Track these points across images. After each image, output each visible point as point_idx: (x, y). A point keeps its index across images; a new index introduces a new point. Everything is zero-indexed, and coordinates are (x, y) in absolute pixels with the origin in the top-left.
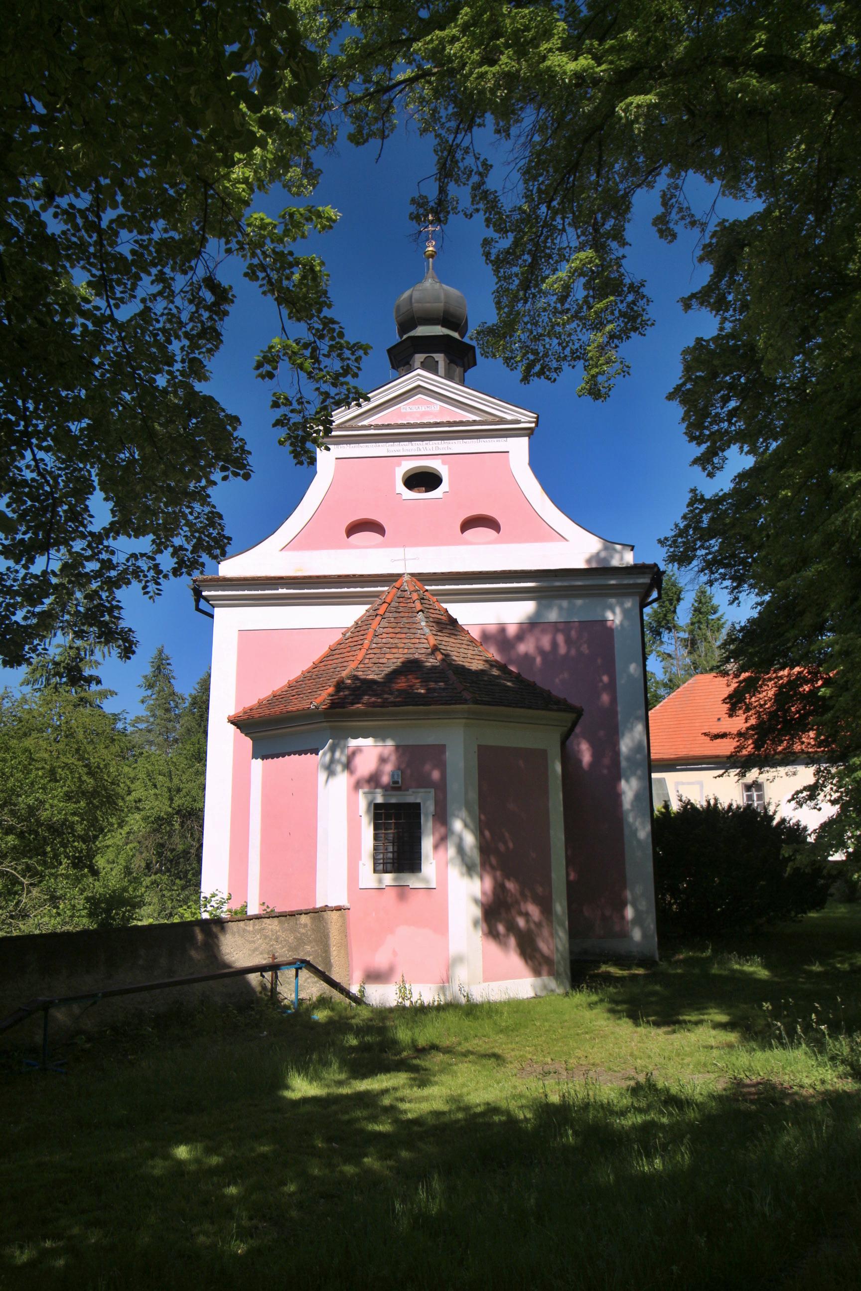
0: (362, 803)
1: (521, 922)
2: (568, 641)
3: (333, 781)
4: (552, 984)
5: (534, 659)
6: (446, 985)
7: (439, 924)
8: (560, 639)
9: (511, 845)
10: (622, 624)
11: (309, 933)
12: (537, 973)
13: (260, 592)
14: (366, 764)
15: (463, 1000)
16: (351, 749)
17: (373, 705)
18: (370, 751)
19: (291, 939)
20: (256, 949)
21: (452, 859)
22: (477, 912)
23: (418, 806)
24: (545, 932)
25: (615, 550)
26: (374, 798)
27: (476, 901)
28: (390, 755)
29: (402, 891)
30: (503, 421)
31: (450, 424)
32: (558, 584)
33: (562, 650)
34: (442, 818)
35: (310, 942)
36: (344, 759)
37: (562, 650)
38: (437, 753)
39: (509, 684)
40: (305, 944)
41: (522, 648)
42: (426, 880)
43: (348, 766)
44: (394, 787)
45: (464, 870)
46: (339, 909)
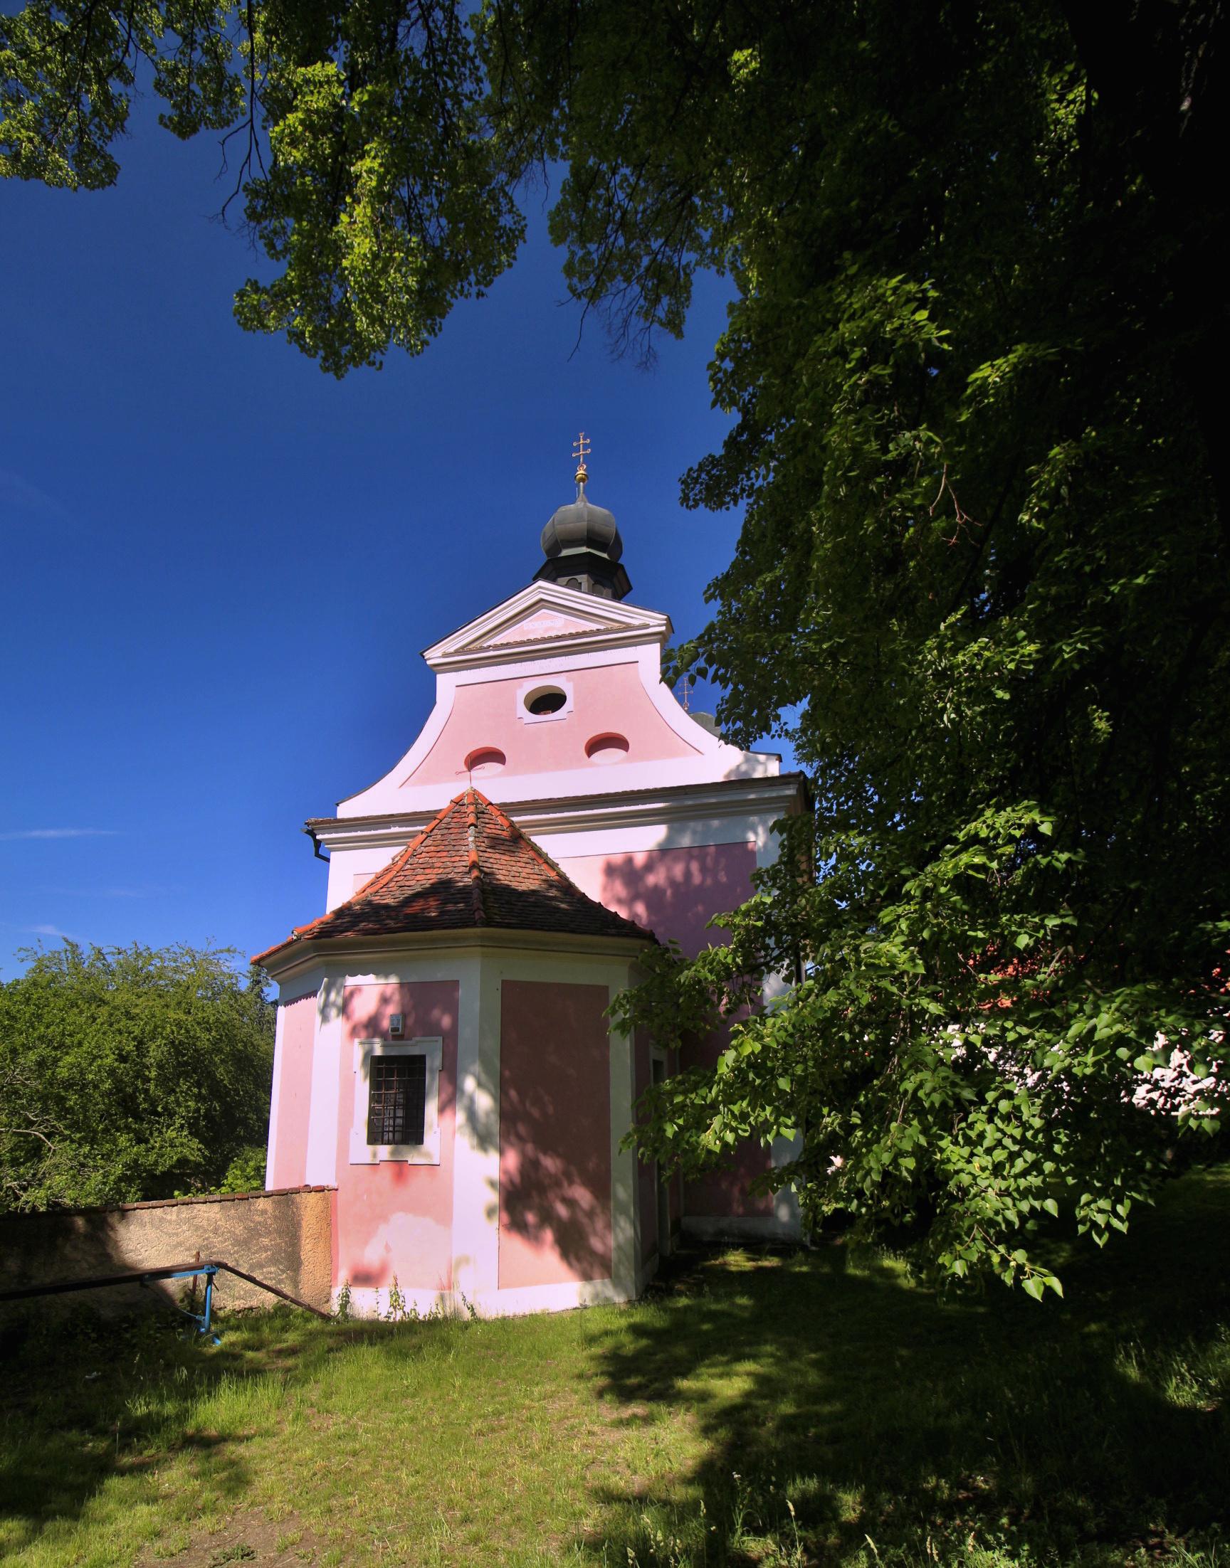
0: (358, 1052)
1: (562, 1211)
2: (703, 870)
3: (326, 1027)
4: (610, 1291)
5: (664, 891)
6: (446, 1292)
7: (441, 1211)
8: (695, 867)
9: (550, 1110)
10: (765, 845)
11: (269, 1222)
12: (587, 1277)
13: (373, 832)
14: (364, 1006)
15: (467, 1315)
16: (348, 990)
17: (367, 932)
18: (371, 991)
19: (239, 1230)
20: (180, 1244)
21: (460, 1127)
22: (493, 1198)
23: (421, 1059)
24: (600, 1224)
25: (758, 762)
26: (371, 1050)
27: (492, 1184)
28: (393, 993)
29: (400, 1169)
30: (629, 627)
31: (572, 636)
32: (690, 803)
33: (697, 879)
34: (452, 1075)
35: (270, 1233)
36: (340, 1001)
37: (697, 879)
38: (446, 993)
39: (563, 906)
40: (260, 1236)
41: (651, 880)
42: (428, 1155)
43: (344, 1010)
44: (397, 1035)
45: (475, 1141)
46: (321, 1190)
